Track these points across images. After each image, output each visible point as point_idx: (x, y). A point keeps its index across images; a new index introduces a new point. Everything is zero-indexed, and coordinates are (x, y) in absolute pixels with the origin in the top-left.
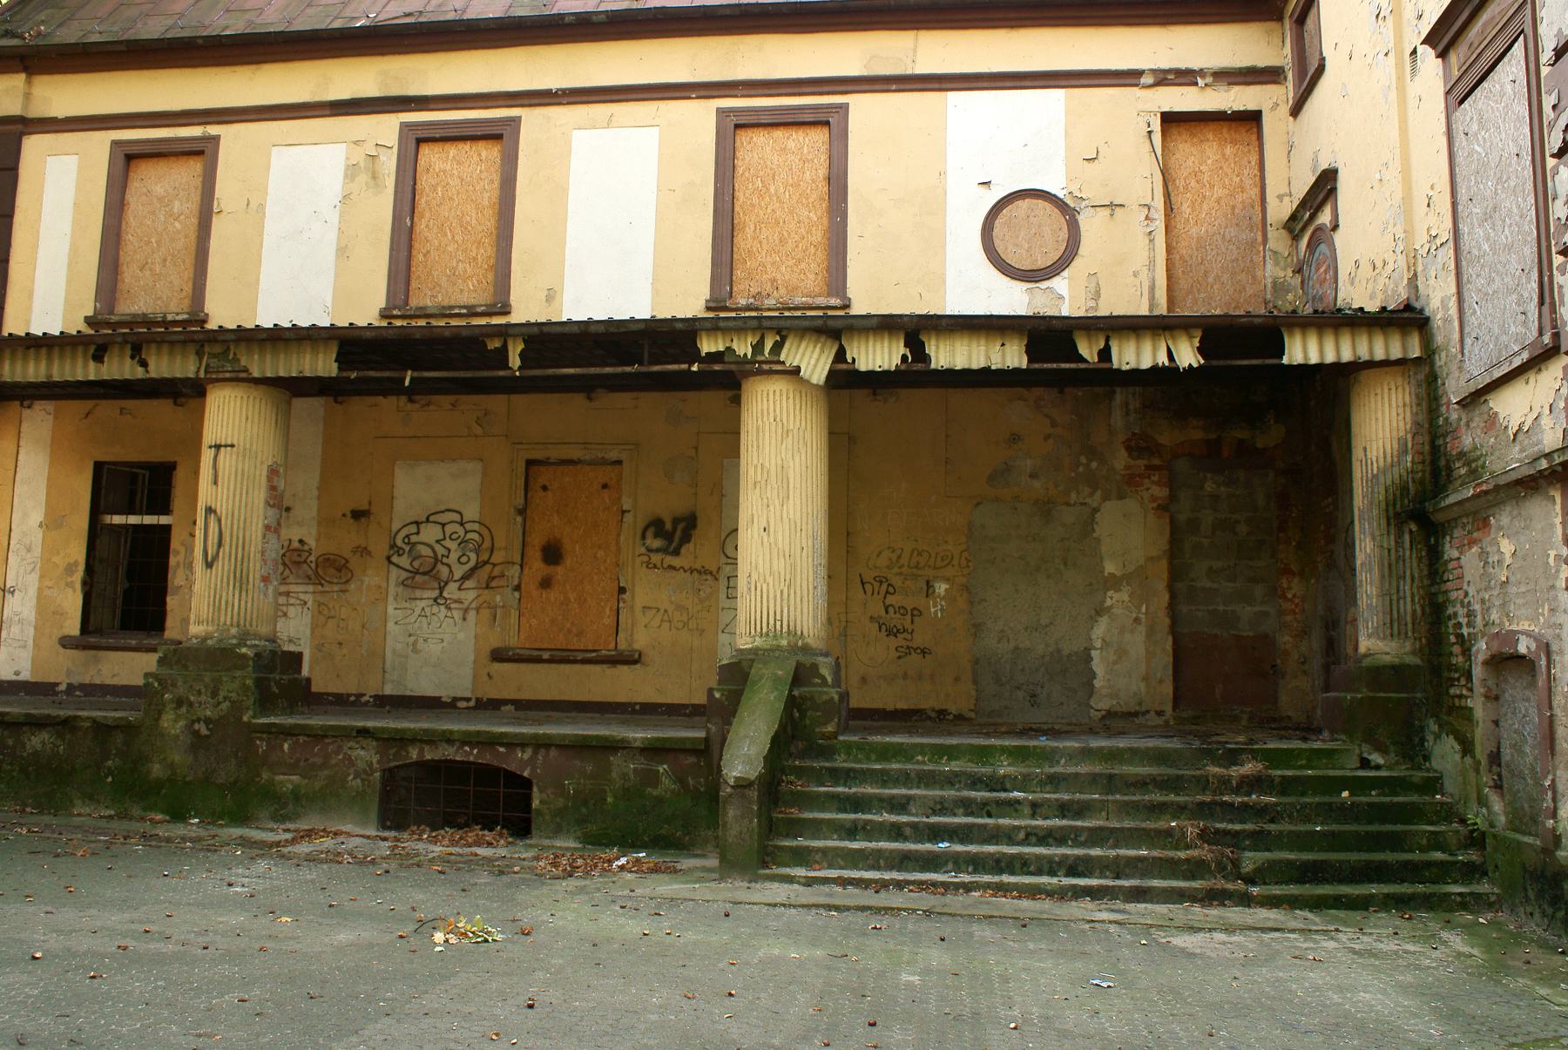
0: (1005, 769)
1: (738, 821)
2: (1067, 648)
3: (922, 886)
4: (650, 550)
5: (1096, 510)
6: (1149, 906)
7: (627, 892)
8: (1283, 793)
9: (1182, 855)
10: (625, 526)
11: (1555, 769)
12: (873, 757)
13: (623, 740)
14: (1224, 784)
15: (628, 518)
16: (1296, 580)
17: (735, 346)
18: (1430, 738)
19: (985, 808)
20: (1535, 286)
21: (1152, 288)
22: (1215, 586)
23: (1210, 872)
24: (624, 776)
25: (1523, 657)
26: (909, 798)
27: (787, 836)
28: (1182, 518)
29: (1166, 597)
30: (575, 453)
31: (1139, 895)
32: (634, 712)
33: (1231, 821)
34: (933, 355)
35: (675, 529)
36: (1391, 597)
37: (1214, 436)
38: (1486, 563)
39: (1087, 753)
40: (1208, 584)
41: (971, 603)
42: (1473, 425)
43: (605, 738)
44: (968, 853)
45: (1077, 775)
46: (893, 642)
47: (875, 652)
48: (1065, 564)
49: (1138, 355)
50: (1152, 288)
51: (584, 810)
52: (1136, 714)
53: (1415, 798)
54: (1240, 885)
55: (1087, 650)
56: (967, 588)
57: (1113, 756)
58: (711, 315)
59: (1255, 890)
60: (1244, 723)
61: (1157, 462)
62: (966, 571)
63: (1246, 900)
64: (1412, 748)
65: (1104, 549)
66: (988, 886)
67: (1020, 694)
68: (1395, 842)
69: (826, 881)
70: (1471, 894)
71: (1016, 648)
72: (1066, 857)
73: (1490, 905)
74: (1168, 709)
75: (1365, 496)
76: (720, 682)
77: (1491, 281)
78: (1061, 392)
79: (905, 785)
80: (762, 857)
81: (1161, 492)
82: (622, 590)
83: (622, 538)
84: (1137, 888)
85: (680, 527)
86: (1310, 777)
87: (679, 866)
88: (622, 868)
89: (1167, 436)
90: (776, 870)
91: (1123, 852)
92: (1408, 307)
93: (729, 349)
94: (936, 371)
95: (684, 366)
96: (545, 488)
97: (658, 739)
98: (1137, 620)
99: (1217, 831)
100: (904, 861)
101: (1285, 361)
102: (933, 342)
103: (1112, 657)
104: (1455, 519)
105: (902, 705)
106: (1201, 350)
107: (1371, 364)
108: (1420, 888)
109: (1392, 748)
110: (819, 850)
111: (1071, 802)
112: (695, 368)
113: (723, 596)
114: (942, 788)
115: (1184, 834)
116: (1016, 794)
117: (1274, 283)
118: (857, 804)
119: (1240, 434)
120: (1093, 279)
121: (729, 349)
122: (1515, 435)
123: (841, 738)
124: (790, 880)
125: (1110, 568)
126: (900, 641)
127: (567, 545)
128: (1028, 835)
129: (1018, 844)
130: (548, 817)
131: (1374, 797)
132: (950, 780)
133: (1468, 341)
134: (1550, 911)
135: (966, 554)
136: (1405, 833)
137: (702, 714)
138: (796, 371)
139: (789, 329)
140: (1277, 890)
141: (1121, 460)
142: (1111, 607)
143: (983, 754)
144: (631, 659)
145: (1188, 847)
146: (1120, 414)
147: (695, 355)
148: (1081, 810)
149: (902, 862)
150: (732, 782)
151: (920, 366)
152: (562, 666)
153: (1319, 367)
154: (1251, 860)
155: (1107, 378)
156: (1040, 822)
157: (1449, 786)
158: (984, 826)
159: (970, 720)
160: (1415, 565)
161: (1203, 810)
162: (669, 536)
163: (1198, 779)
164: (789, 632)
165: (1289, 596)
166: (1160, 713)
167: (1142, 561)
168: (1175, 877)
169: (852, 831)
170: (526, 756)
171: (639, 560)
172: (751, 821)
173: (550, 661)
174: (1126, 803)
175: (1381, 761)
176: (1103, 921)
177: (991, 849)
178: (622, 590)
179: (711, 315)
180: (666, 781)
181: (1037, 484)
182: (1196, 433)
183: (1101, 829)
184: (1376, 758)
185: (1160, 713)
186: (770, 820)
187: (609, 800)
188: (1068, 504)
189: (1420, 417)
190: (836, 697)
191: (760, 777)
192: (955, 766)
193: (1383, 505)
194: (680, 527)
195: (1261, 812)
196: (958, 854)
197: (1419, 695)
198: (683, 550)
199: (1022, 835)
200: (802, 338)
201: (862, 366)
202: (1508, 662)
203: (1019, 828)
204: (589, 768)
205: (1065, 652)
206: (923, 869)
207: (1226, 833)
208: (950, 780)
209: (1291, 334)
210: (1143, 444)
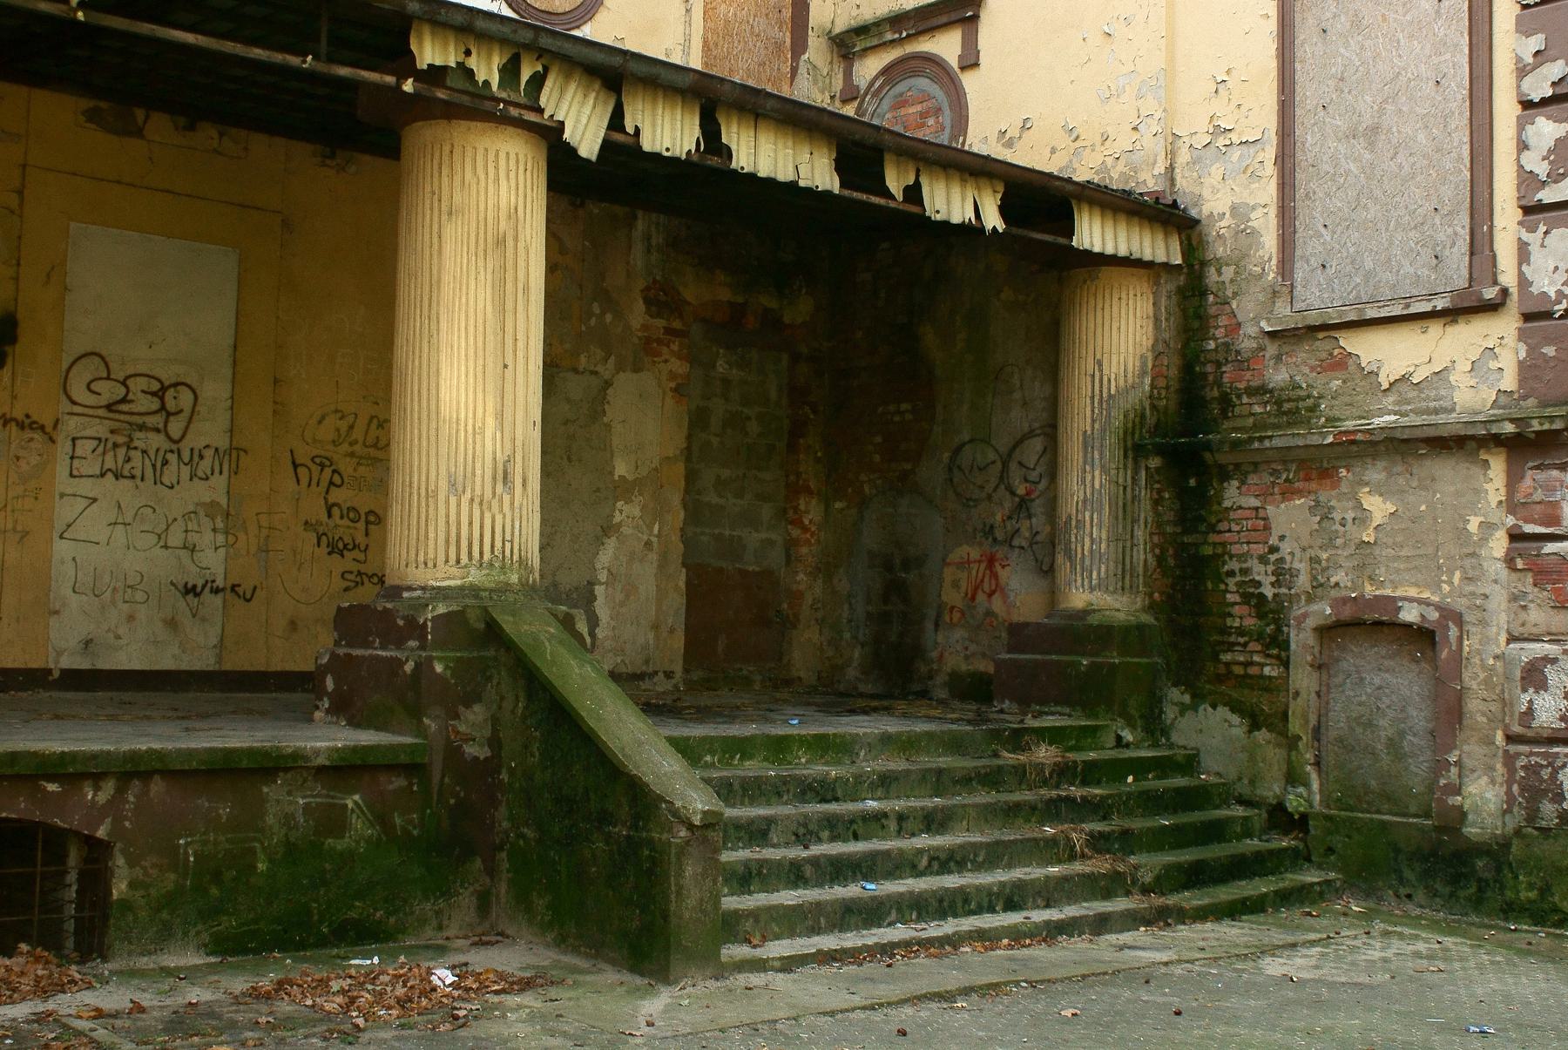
5: (608, 384)
14: (1020, 773)
16: (814, 502)
17: (472, 62)
22: (722, 501)
24: (288, 820)
26: (770, 821)
34: (734, 147)
37: (740, 300)
40: (715, 500)
46: (338, 564)
48: (569, 460)
51: (214, 891)
61: (677, 324)
65: (616, 441)
74: (678, 668)
81: (679, 367)
89: (693, 291)
95: (390, 79)
98: (648, 544)
102: (734, 128)
103: (619, 597)
112: (408, 86)
113: (62, 470)
119: (772, 303)
125: (621, 469)
126: (348, 562)
128: (932, 859)
130: (143, 914)
141: (637, 315)
142: (620, 525)
147: (403, 61)
151: (714, 161)
157: (1207, 761)
166: (669, 675)
167: (656, 463)
170: (102, 798)
185: (669, 675)
188: (576, 371)
189: (1166, 336)
203: (920, 852)
204: (224, 811)
210: (662, 297)
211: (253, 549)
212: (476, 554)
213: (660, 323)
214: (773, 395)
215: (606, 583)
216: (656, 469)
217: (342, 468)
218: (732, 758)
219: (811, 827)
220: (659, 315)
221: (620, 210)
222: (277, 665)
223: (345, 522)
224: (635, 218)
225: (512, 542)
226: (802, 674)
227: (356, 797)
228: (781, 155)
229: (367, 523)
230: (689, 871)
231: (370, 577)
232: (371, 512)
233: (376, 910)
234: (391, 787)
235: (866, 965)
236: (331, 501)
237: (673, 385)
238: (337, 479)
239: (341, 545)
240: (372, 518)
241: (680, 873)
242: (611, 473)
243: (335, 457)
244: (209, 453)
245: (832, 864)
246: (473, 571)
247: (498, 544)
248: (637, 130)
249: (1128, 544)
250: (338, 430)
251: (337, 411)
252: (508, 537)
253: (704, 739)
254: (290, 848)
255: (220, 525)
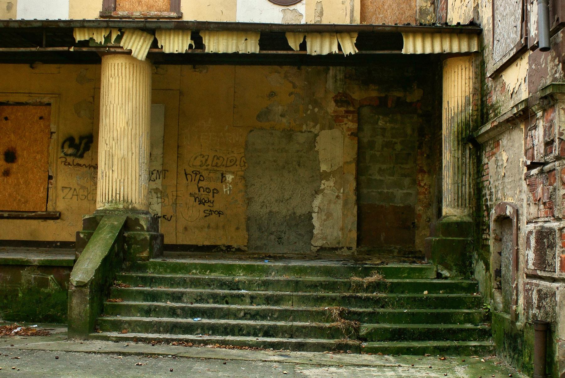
0: (241, 277)
1: (79, 307)
2: (299, 212)
3: (180, 342)
4: (66, 155)
5: (316, 135)
6: (303, 353)
7: (9, 346)
8: (392, 292)
9: (328, 325)
10: (52, 141)
11: (518, 278)
12: (168, 270)
13: (28, 261)
14: (359, 287)
15: (54, 136)
16: (426, 176)
17: (95, 37)
18: (474, 262)
19: (224, 299)
20: (520, 11)
21: (352, 11)
23: (342, 334)
24: (29, 282)
25: (509, 217)
26: (183, 294)
27: (112, 314)
28: (365, 140)
29: (354, 184)
30: (24, 99)
31: (300, 347)
32: (56, 247)
33: (360, 307)
34: (206, 44)
35: (80, 143)
36: (459, 185)
37: (383, 95)
38: (497, 166)
39: (287, 269)
40: (378, 177)
41: (246, 186)
42: (497, 89)
43: (17, 260)
44: (209, 323)
45: (278, 281)
47: (192, 213)
48: (299, 165)
49: (321, 47)
50: (352, 11)
51: (5, 301)
52: (336, 249)
53: (463, 295)
54: (357, 342)
55: (310, 213)
56: (244, 178)
57: (302, 271)
58: (102, 19)
59: (364, 345)
60: (395, 254)
61: (351, 109)
62: (243, 168)
63: (358, 350)
64: (466, 268)
65: (321, 157)
66: (217, 342)
67: (273, 237)
68: (446, 318)
69: (127, 339)
70: (480, 346)
71: (271, 212)
72: (263, 326)
73: (490, 352)
74: (354, 245)
75: (448, 130)
76: (84, 229)
77: (505, 9)
78: (299, 68)
79: (183, 286)
80: (93, 327)
81: (353, 126)
82: (50, 178)
83: (50, 148)
84: (299, 343)
85: (84, 142)
86: (406, 283)
87: (52, 332)
88: (16, 333)
89: (357, 95)
90: (101, 334)
91: (295, 323)
92: (472, 23)
93: (91, 39)
94: (208, 54)
95: (66, 48)
96: (6, 119)
97: (48, 260)
99: (350, 312)
100: (173, 328)
101: (403, 52)
103: (324, 217)
104: (487, 142)
105: (207, 243)
106: (356, 45)
107: (451, 55)
108: (455, 343)
109: (454, 268)
110: (127, 322)
111: (272, 296)
114: (204, 288)
115: (331, 314)
116: (243, 291)
117: (420, 9)
118: (154, 297)
120: (319, 5)
121: (91, 39)
122: (512, 95)
123: (151, 260)
124: (107, 339)
125: (324, 167)
126: (206, 207)
127: (19, 152)
128: (245, 314)
129: (240, 319)
131: (441, 294)
132: (208, 284)
133: (495, 42)
134: (512, 354)
135: (243, 159)
136: (452, 314)
137: (74, 247)
138: (129, 52)
139: (126, 28)
140: (376, 344)
141: (331, 107)
142: (324, 189)
143: (229, 269)
144: (55, 216)
145: (333, 321)
146: (333, 79)
147: (72, 42)
148: (278, 300)
149: (172, 329)
150: (74, 284)
151: (199, 51)
152: (15, 221)
153: (423, 56)
154: (366, 328)
155: (304, 60)
156: (254, 307)
157: (481, 289)
158: (221, 309)
159: (244, 251)
160: (471, 167)
161: (345, 300)
162: (77, 147)
163: (345, 284)
164: (124, 200)
165: (422, 184)
166: (349, 248)
168: (323, 337)
169: (148, 312)
171: (60, 160)
172: (86, 307)
173: (8, 218)
174: (303, 297)
175: (448, 274)
176: (271, 361)
177: (223, 321)
178: (50, 178)
179: (102, 19)
180: (52, 284)
181: (284, 120)
182: (374, 93)
183: (286, 311)
184: (446, 273)
185: (349, 248)
186: (102, 305)
187: (20, 295)
188: (301, 132)
190: (148, 237)
191: (92, 281)
192: (213, 276)
193: (456, 133)
194: (84, 142)
195: (377, 302)
196: (204, 324)
197: (470, 239)
198: (85, 155)
199: (242, 314)
200: (133, 34)
201: (167, 50)
202: (504, 221)
203: (241, 310)
204: (8, 277)
205: (298, 215)
206: (184, 333)
207: (355, 313)
208: (208, 284)
209: (407, 37)
211: (170, 204)
212: (107, 199)
213: (343, 109)
214: (409, 131)
215: (318, 212)
216: (341, 167)
217: (203, 174)
218: (206, 271)
219: (203, 297)
220: (342, 106)
221: (320, 68)
222: (180, 242)
223: (205, 193)
224: (329, 69)
225: (120, 194)
226: (421, 249)
227: (52, 276)
228: (230, 43)
229: (213, 193)
230: (74, 301)
231: (214, 212)
232: (215, 189)
233: (58, 312)
234: (64, 274)
235: (156, 347)
236: (200, 185)
237: (350, 133)
238: (202, 178)
239: (203, 201)
240: (215, 191)
241: (71, 302)
242: (319, 170)
243: (201, 171)
244: (155, 172)
245: (191, 310)
246: (106, 204)
247: (114, 195)
248: (162, 46)
249: (460, 185)
250: (202, 161)
251: (201, 155)
252: (118, 192)
253: (191, 264)
254: (30, 290)
255: (159, 195)
